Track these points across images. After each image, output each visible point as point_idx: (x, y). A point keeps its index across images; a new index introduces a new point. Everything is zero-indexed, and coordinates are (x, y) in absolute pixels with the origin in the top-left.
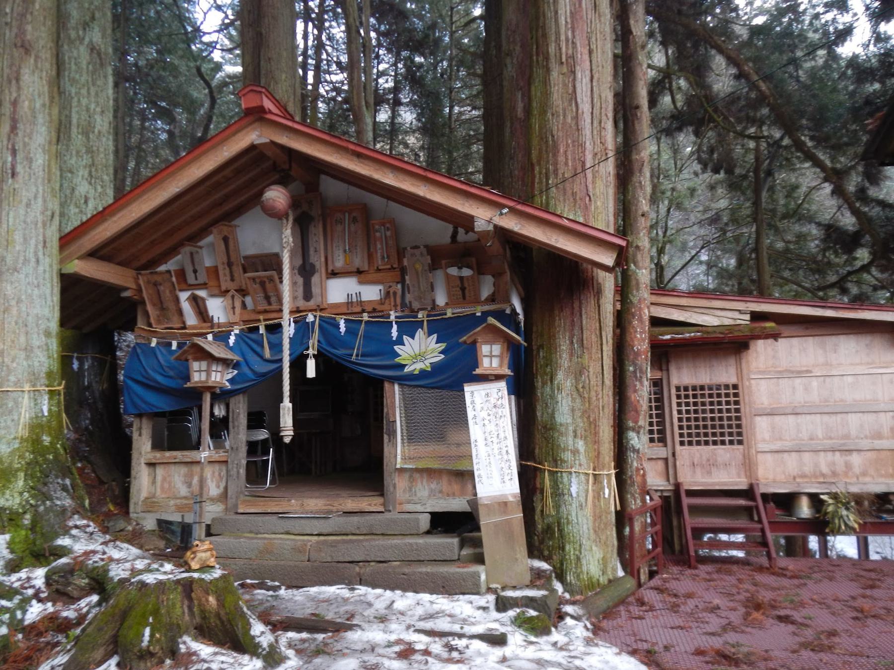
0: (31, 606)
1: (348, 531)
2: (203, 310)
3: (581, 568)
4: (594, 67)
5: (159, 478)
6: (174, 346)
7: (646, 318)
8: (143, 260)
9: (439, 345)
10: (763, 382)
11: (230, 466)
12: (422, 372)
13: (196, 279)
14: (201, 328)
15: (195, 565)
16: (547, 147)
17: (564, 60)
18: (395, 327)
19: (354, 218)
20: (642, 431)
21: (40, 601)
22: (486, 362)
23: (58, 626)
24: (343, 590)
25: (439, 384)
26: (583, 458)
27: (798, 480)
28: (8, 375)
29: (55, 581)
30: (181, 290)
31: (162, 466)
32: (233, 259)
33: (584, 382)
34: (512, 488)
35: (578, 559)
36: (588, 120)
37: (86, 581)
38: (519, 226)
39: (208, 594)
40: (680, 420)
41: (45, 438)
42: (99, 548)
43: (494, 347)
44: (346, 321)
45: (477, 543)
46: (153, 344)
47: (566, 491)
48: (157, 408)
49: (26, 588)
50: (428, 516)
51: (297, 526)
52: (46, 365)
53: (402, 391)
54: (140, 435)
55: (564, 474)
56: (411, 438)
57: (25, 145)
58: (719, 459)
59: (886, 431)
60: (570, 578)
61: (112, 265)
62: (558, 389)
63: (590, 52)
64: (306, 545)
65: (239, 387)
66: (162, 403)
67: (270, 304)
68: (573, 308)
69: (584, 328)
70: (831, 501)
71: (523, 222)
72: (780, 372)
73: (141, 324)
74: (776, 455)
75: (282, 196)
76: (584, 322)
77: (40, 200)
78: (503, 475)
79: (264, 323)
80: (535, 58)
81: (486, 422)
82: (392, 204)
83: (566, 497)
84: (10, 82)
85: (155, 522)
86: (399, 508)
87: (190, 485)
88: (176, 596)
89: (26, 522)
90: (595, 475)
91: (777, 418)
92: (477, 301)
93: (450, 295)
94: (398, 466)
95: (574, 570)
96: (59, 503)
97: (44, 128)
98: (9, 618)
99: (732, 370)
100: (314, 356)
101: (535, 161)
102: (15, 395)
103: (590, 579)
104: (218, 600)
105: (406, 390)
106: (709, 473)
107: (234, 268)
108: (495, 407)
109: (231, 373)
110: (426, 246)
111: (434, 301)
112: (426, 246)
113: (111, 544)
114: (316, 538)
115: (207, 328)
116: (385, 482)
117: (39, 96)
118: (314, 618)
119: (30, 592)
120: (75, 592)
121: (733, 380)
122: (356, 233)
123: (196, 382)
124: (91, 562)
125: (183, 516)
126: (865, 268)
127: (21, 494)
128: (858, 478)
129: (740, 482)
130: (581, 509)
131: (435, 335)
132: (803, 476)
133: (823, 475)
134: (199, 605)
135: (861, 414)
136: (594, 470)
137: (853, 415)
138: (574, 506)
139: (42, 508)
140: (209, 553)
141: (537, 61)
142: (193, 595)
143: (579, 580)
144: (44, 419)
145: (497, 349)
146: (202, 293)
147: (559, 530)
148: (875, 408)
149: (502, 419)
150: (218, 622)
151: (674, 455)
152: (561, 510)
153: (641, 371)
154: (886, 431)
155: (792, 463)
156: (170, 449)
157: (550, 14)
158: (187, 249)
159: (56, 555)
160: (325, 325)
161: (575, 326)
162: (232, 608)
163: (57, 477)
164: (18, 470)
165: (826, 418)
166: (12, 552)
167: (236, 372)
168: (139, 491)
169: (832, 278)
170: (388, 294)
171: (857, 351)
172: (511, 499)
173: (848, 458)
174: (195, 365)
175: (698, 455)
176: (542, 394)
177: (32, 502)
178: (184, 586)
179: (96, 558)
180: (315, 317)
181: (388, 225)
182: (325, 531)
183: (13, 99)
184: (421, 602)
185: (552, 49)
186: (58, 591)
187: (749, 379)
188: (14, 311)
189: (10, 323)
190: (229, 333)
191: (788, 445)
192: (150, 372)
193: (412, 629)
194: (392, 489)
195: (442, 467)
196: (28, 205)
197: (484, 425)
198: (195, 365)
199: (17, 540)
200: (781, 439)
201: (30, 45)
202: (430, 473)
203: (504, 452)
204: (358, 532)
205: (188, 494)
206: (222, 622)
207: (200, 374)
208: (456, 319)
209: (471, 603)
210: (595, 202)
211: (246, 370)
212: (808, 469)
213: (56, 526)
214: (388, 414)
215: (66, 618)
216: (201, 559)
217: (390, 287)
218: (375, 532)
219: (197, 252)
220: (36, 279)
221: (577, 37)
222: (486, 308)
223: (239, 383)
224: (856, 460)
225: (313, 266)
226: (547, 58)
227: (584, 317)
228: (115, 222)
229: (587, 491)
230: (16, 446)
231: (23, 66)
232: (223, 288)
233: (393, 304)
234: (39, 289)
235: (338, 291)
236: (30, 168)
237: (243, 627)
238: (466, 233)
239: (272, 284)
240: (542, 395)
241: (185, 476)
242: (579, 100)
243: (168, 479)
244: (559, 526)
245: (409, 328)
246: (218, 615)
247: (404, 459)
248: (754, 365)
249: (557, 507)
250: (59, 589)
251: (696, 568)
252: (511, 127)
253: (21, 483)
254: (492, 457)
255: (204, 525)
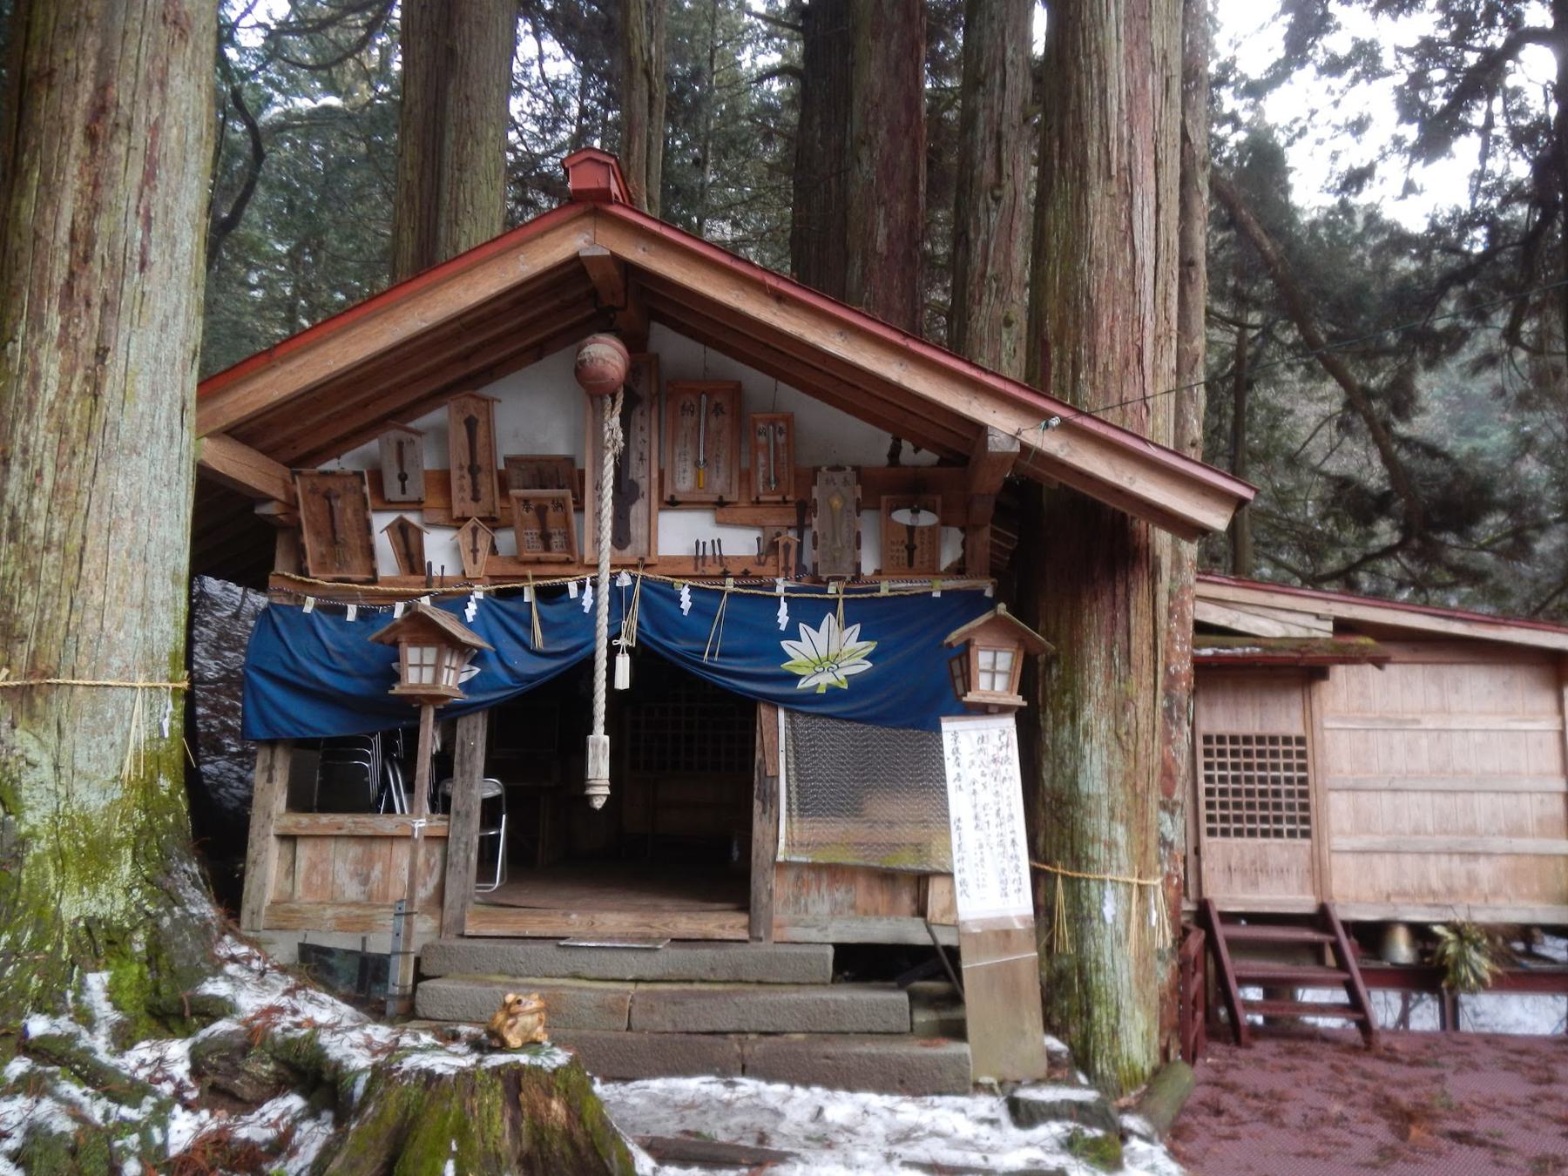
0: (174, 1118)
1: (693, 975)
2: (414, 549)
3: (1119, 1047)
4: (1162, 191)
5: (302, 864)
6: (352, 614)
7: (1190, 619)
8: (303, 449)
9: (864, 644)
10: (1343, 735)
11: (452, 848)
12: (833, 691)
13: (403, 491)
14: (406, 584)
15: (514, 1040)
16: (1077, 316)
17: (1114, 172)
18: (784, 606)
19: (717, 405)
20: (1178, 812)
21: (187, 1106)
22: (983, 682)
23: (232, 1158)
24: (714, 1087)
25: (854, 715)
26: (1122, 856)
27: (1393, 899)
28: (109, 656)
29: (212, 1067)
30: (375, 510)
31: (311, 842)
32: (481, 460)
33: (1129, 725)
34: (1018, 905)
35: (1114, 1032)
36: (1150, 279)
37: (271, 1067)
38: (1066, 450)
39: (551, 1096)
40: (1209, 792)
41: (162, 781)
42: (284, 1001)
43: (1000, 656)
44: (693, 589)
45: (955, 999)
46: (308, 609)
47: (1094, 913)
48: (312, 729)
49: (159, 1082)
50: (830, 951)
51: (591, 964)
52: (171, 638)
53: (792, 722)
54: (270, 780)
55: (1092, 884)
56: (805, 806)
57: (167, 210)
58: (1271, 862)
59: (1530, 824)
60: (1101, 1066)
61: (254, 453)
62: (1086, 734)
63: (1157, 165)
64: (624, 1000)
65: (481, 698)
66: (320, 721)
67: (548, 548)
68: (1114, 595)
69: (1133, 631)
70: (1451, 937)
71: (1074, 443)
72: (1371, 720)
73: (282, 566)
74: (1361, 858)
75: (618, 357)
76: (1133, 621)
77: (181, 318)
78: (1004, 882)
79: (533, 583)
80: (1056, 162)
81: (978, 787)
82: (782, 386)
83: (1095, 923)
84: (150, 88)
85: (296, 950)
86: (777, 934)
87: (365, 880)
88: (493, 1100)
89: (138, 948)
90: (1140, 886)
91: (1363, 796)
92: (933, 571)
93: (885, 554)
94: (780, 858)
95: (1107, 1052)
96: (194, 911)
97: (196, 183)
98: (140, 1143)
99: (1296, 713)
100: (630, 650)
101: (1051, 337)
102: (119, 693)
103: (1132, 1067)
104: (568, 1107)
105: (799, 720)
106: (1255, 884)
107: (483, 478)
108: (995, 761)
109: (471, 672)
110: (856, 469)
111: (858, 566)
112: (856, 469)
113: (300, 994)
114: (630, 987)
115: (417, 585)
116: (753, 888)
117: (195, 121)
118: (687, 1138)
119: (167, 1088)
120: (247, 1090)
121: (1296, 730)
122: (719, 432)
123: (413, 686)
124: (278, 1029)
125: (364, 940)
126: (1388, 552)
127: (128, 891)
128: (1486, 900)
129: (1305, 903)
130: (1120, 945)
131: (857, 627)
132: (1403, 894)
133: (1433, 893)
134: (533, 1116)
135: (1492, 796)
136: (1139, 877)
137: (1482, 796)
138: (1108, 939)
139: (166, 921)
140: (536, 1017)
141: (1062, 167)
142: (522, 1097)
143: (1116, 1068)
144: (162, 744)
145: (1005, 660)
146: (413, 518)
147: (1080, 981)
148: (1516, 787)
149: (1007, 783)
150: (567, 1150)
151: (1197, 851)
152: (1086, 946)
153: (1180, 709)
154: (1530, 824)
155: (1385, 872)
156: (324, 808)
157: (1090, 92)
158: (393, 435)
159: (207, 1014)
160: (652, 594)
161: (1120, 628)
162: (597, 1123)
163: (181, 860)
164: (120, 844)
165: (1439, 799)
166: (117, 1007)
167: (477, 670)
168: (262, 887)
169: (1333, 563)
170: (773, 546)
171: (1490, 693)
172: (1019, 926)
173: (1472, 866)
174: (412, 654)
175: (1237, 853)
176: (1054, 741)
177: (148, 907)
178: (505, 1080)
179: (287, 1020)
180: (634, 578)
181: (781, 424)
182: (648, 974)
183: (152, 120)
184: (871, 1110)
185: (1093, 152)
186: (215, 1089)
187: (1323, 729)
188: (127, 529)
189: (117, 552)
190: (464, 599)
191: (1379, 841)
192: (301, 659)
193: (896, 1162)
194: (764, 898)
195: (862, 862)
196: (163, 327)
197: (974, 792)
198: (412, 654)
199: (125, 984)
200: (1369, 831)
201: (188, 25)
202: (834, 872)
203: (1008, 842)
204: (712, 977)
205: (362, 898)
206: (575, 1147)
207: (420, 671)
208: (897, 600)
209: (963, 1110)
210: (1155, 418)
211: (496, 667)
212: (1409, 883)
213: (198, 958)
214: (763, 762)
215: (247, 1141)
216: (524, 1028)
217: (779, 535)
218: (744, 978)
219: (412, 442)
220: (167, 470)
221: (1138, 138)
222: (951, 584)
223: (482, 692)
224: (1484, 868)
225: (634, 486)
226: (1083, 165)
227: (1132, 612)
228: (291, 372)
229: (1129, 913)
230: (118, 795)
231: (173, 60)
232: (457, 513)
233: (781, 564)
234: (170, 490)
235: (679, 534)
236: (171, 256)
237: (620, 1160)
238: (917, 450)
239: (560, 513)
240: (1054, 741)
241: (358, 862)
242: (1137, 242)
243: (320, 867)
244: (1081, 973)
245: (810, 611)
246: (568, 1136)
247: (790, 845)
248: (1329, 705)
249: (1079, 939)
250: (219, 1083)
251: (1249, 1047)
252: (863, 267)
253: (127, 870)
254: (986, 850)
255: (412, 957)
